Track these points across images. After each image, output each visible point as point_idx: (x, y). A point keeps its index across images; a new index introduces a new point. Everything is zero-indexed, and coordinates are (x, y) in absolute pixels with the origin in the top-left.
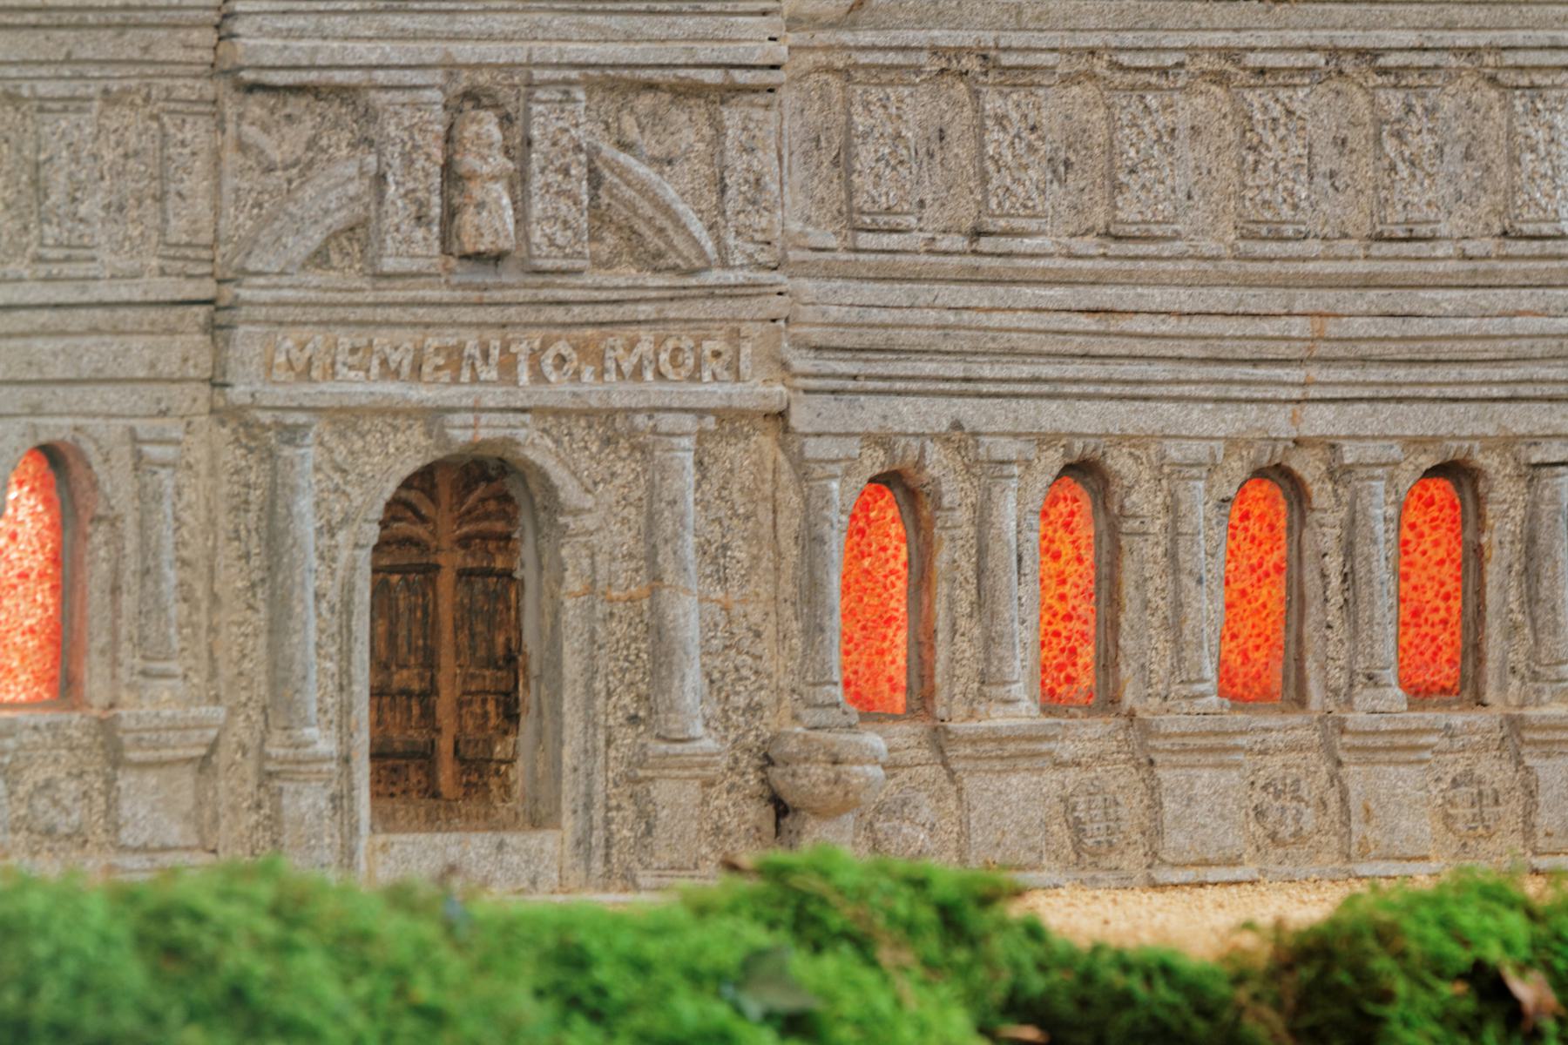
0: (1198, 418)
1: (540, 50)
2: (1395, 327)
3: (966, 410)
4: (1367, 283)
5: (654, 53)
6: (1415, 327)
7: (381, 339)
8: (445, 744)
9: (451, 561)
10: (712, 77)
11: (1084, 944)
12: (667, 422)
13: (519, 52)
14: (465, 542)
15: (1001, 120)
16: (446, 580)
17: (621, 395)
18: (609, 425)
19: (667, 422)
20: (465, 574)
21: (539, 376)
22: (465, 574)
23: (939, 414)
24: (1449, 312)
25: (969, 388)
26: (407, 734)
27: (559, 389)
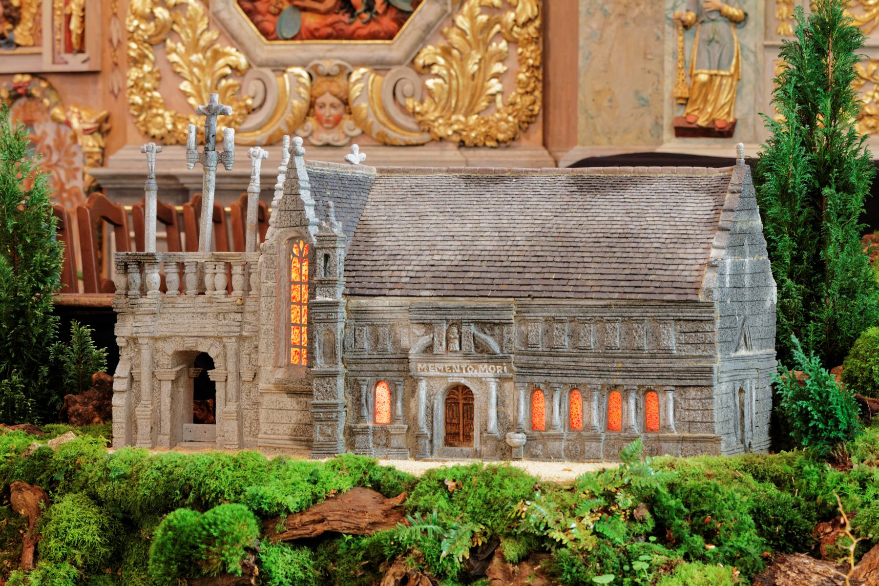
0: (594, 381)
1: (463, 317)
2: (635, 366)
3: (548, 378)
4: (631, 357)
5: (487, 317)
6: (639, 366)
7: (436, 365)
8: (461, 433)
9: (461, 402)
10: (496, 321)
11: (534, 476)
12: (488, 380)
13: (460, 317)
14: (131, 441)
15: (557, 329)
16: (461, 405)
17: (480, 374)
18: (480, 380)
19: (488, 380)
20: (464, 404)
21: (467, 371)
22: (464, 404)
23: (543, 379)
24: (645, 363)
25: (549, 375)
26: (454, 430)
27: (470, 374)
